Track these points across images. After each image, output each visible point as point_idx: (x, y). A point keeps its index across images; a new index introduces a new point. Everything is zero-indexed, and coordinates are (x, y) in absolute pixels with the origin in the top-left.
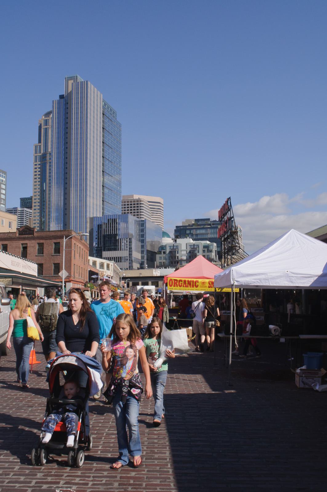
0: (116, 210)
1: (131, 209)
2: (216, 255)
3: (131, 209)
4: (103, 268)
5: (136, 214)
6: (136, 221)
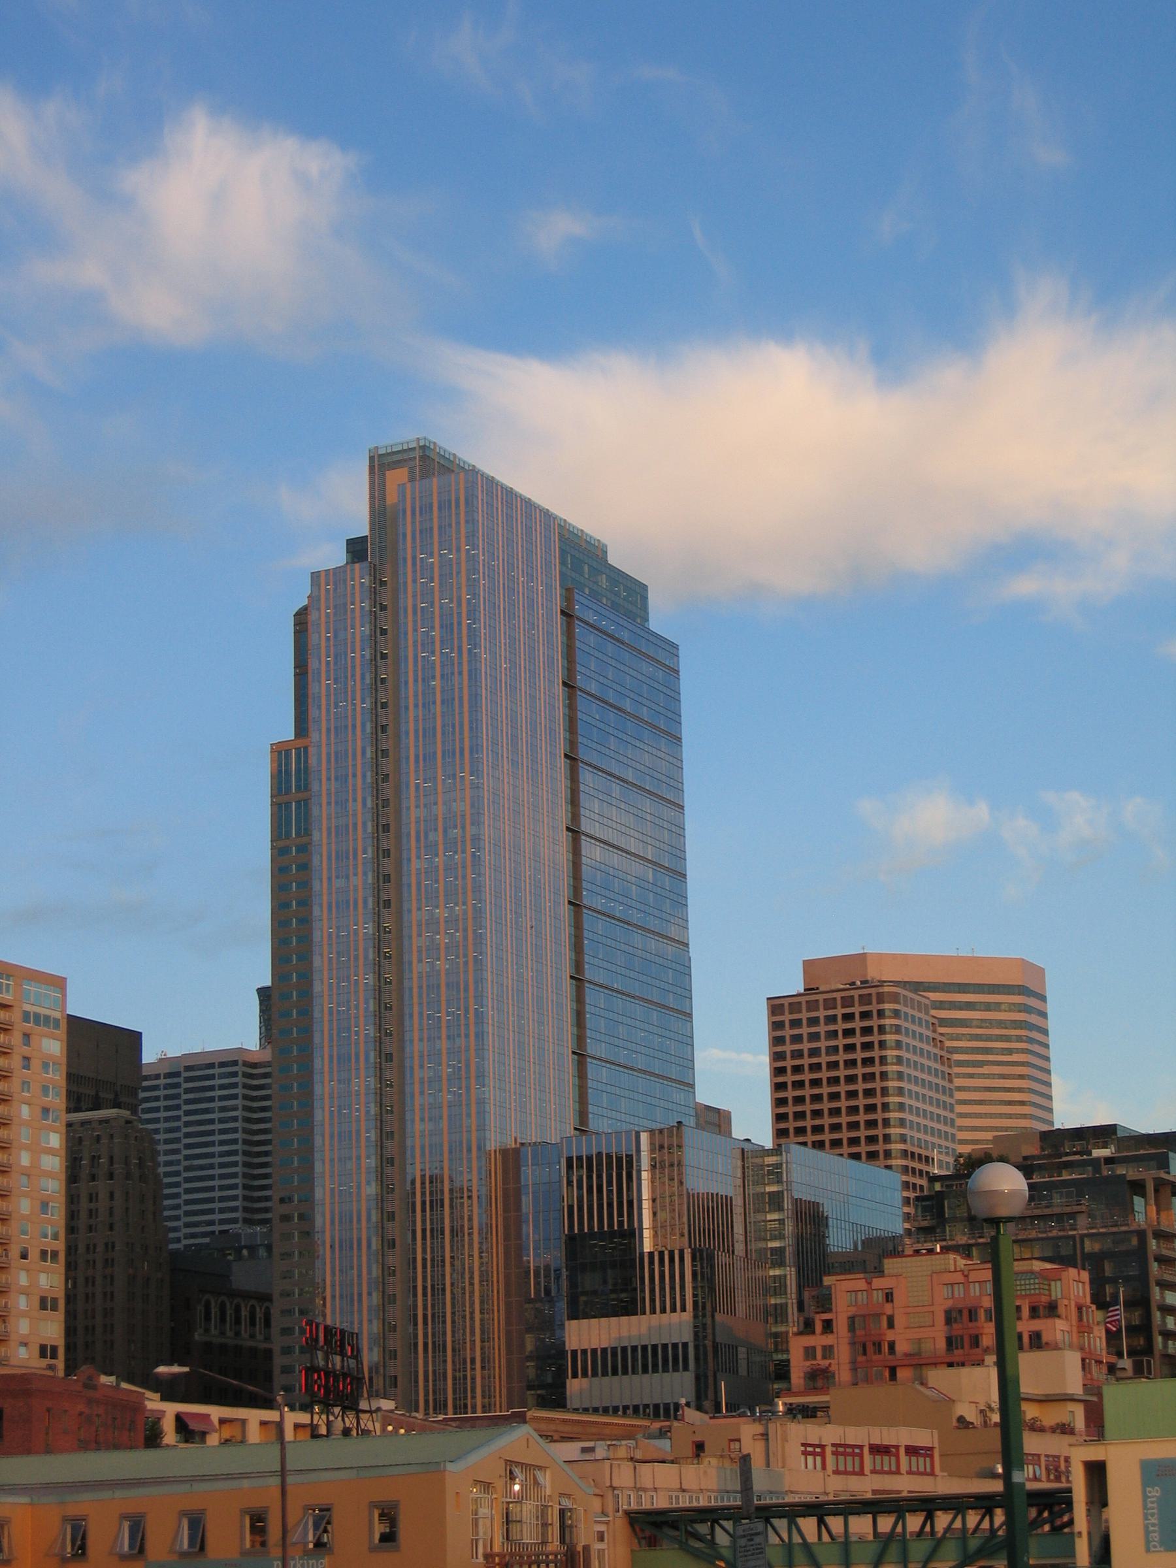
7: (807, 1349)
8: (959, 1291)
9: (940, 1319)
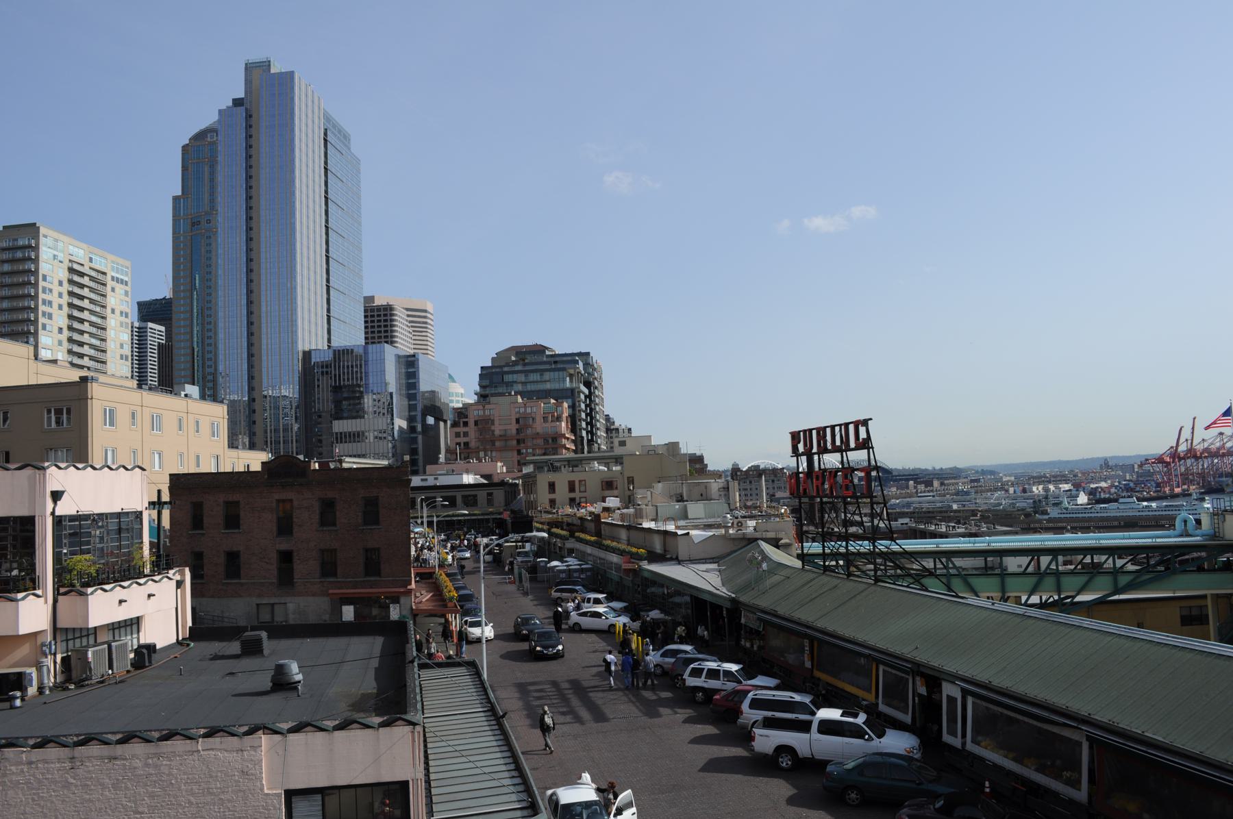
0: (351, 334)
8: (522, 410)
9: (514, 421)
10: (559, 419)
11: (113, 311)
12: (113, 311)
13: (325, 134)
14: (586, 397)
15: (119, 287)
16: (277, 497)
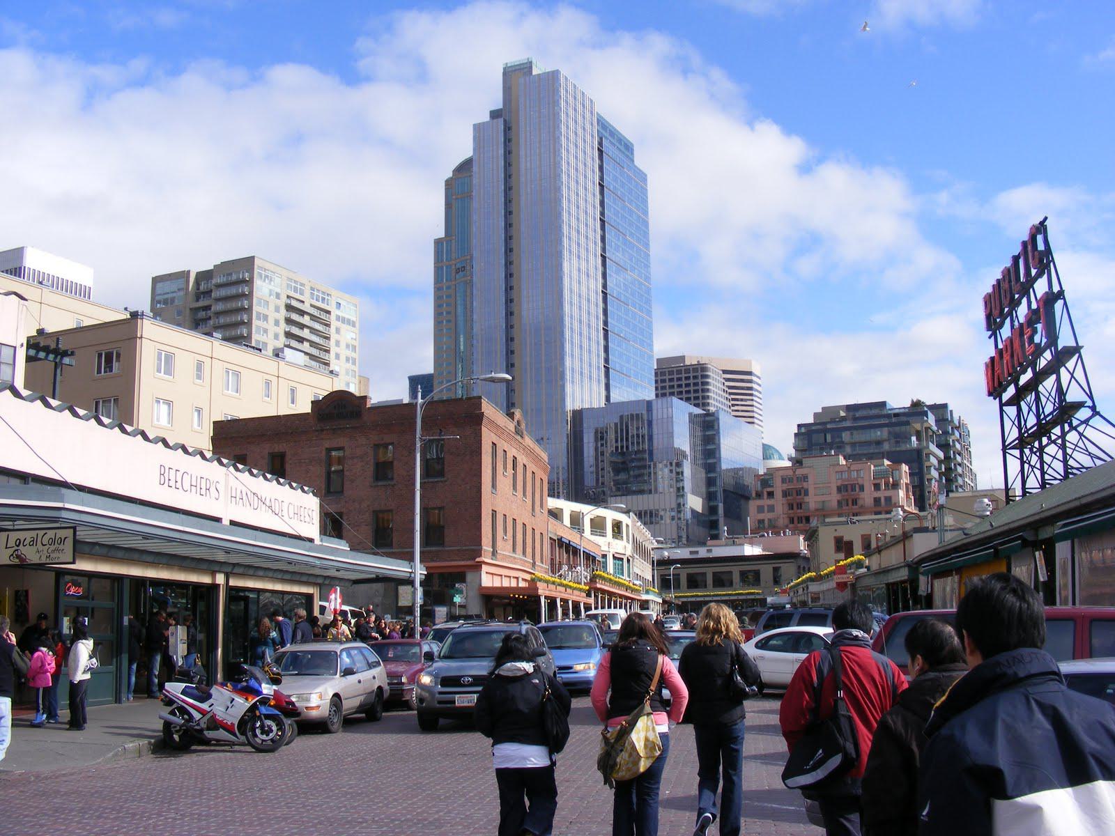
0: (637, 389)
1: (680, 390)
2: (908, 497)
3: (680, 390)
4: (603, 535)
5: (692, 395)
6: (693, 418)
7: (758, 507)
8: (845, 476)
9: (835, 490)
10: (896, 486)
11: (338, 357)
12: (338, 357)
13: (600, 144)
14: (940, 462)
15: (344, 327)
16: (327, 444)
